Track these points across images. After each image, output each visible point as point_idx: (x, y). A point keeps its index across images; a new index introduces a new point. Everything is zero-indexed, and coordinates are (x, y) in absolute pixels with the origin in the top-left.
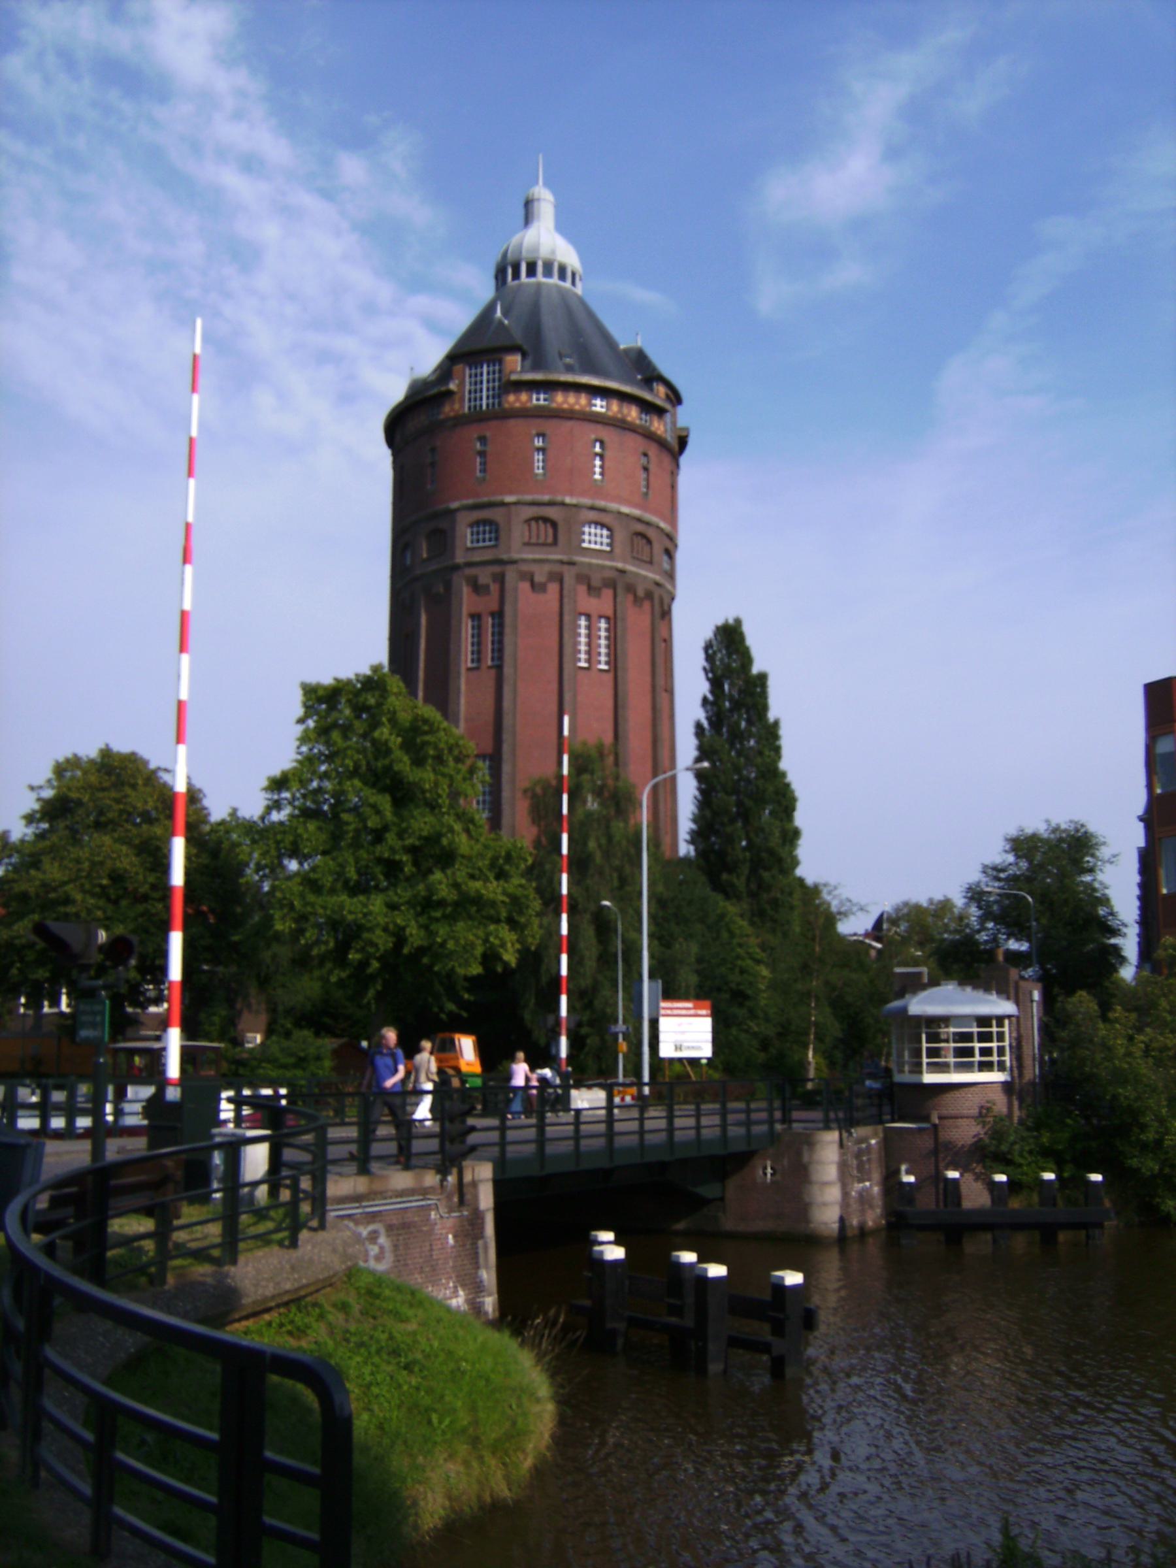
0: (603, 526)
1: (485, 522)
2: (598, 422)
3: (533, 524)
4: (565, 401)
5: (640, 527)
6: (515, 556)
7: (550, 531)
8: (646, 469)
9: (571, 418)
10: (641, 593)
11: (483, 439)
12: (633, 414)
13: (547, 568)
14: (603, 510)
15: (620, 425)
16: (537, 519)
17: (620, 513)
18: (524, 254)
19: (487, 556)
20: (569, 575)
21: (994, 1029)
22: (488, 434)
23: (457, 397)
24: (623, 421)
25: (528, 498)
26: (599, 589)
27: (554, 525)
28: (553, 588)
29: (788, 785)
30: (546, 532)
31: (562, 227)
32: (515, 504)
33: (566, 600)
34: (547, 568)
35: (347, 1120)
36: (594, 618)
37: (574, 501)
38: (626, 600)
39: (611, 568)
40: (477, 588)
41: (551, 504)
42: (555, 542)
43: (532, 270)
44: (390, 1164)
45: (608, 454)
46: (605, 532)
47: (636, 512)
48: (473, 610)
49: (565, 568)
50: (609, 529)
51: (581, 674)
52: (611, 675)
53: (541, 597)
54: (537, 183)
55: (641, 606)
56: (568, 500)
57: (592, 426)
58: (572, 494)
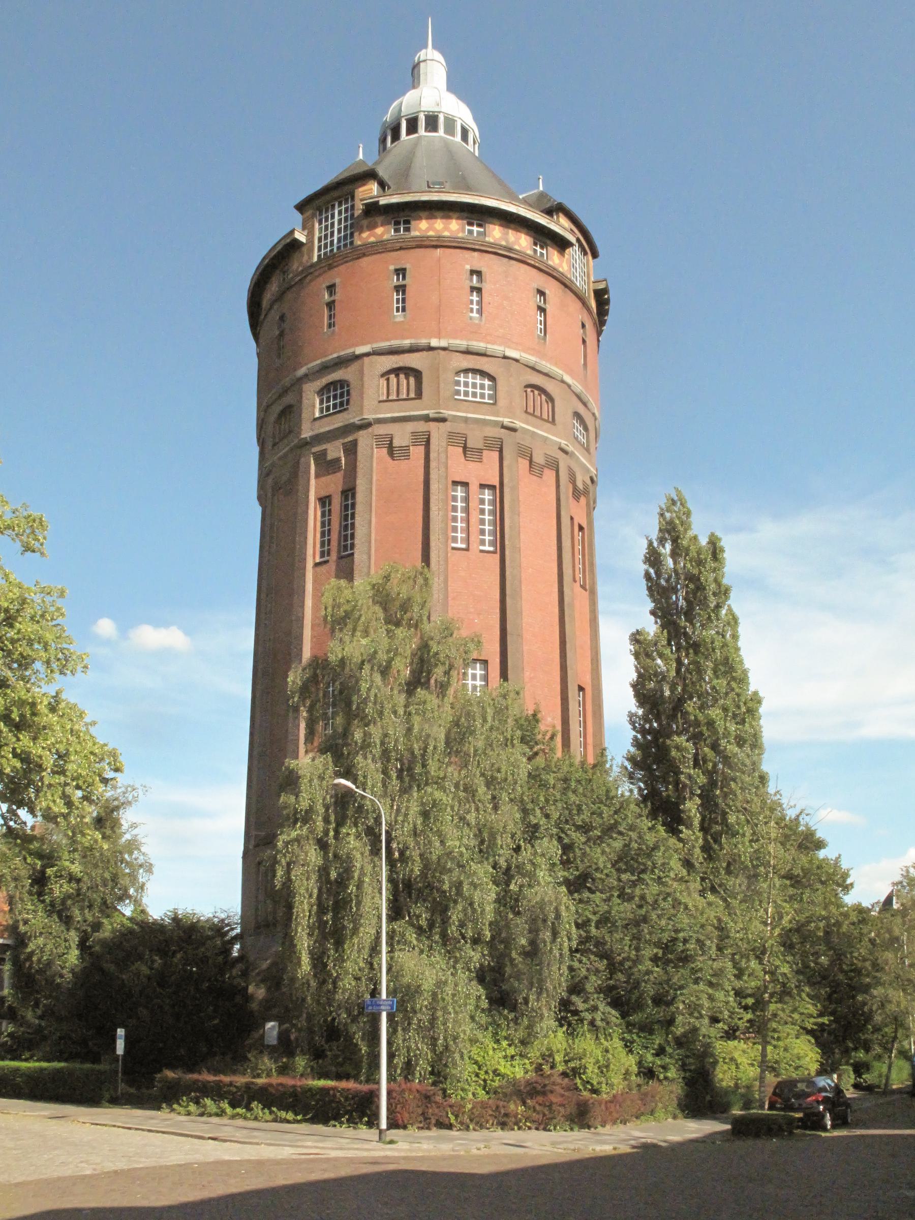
0: (483, 374)
1: (334, 384)
3: (392, 377)
6: (370, 416)
7: (412, 380)
8: (542, 310)
10: (539, 458)
11: (331, 288)
12: (523, 242)
13: (410, 427)
15: (508, 254)
16: (397, 371)
18: (404, 111)
19: (338, 422)
20: (438, 432)
21: (462, 389)
22: (337, 281)
23: (305, 249)
25: (384, 344)
26: (480, 451)
27: (417, 374)
28: (418, 452)
29: (159, 1108)
30: (406, 384)
31: (452, 87)
32: (367, 355)
33: (433, 464)
36: (474, 488)
37: (443, 343)
38: (517, 468)
39: (495, 423)
40: (327, 466)
41: (413, 350)
42: (419, 395)
43: (413, 126)
45: (486, 287)
46: (487, 382)
47: (531, 359)
48: (323, 494)
49: (433, 426)
50: (492, 378)
51: (454, 557)
52: (497, 556)
53: (404, 464)
54: (426, 47)
55: (540, 476)
56: (434, 343)
57: (467, 254)
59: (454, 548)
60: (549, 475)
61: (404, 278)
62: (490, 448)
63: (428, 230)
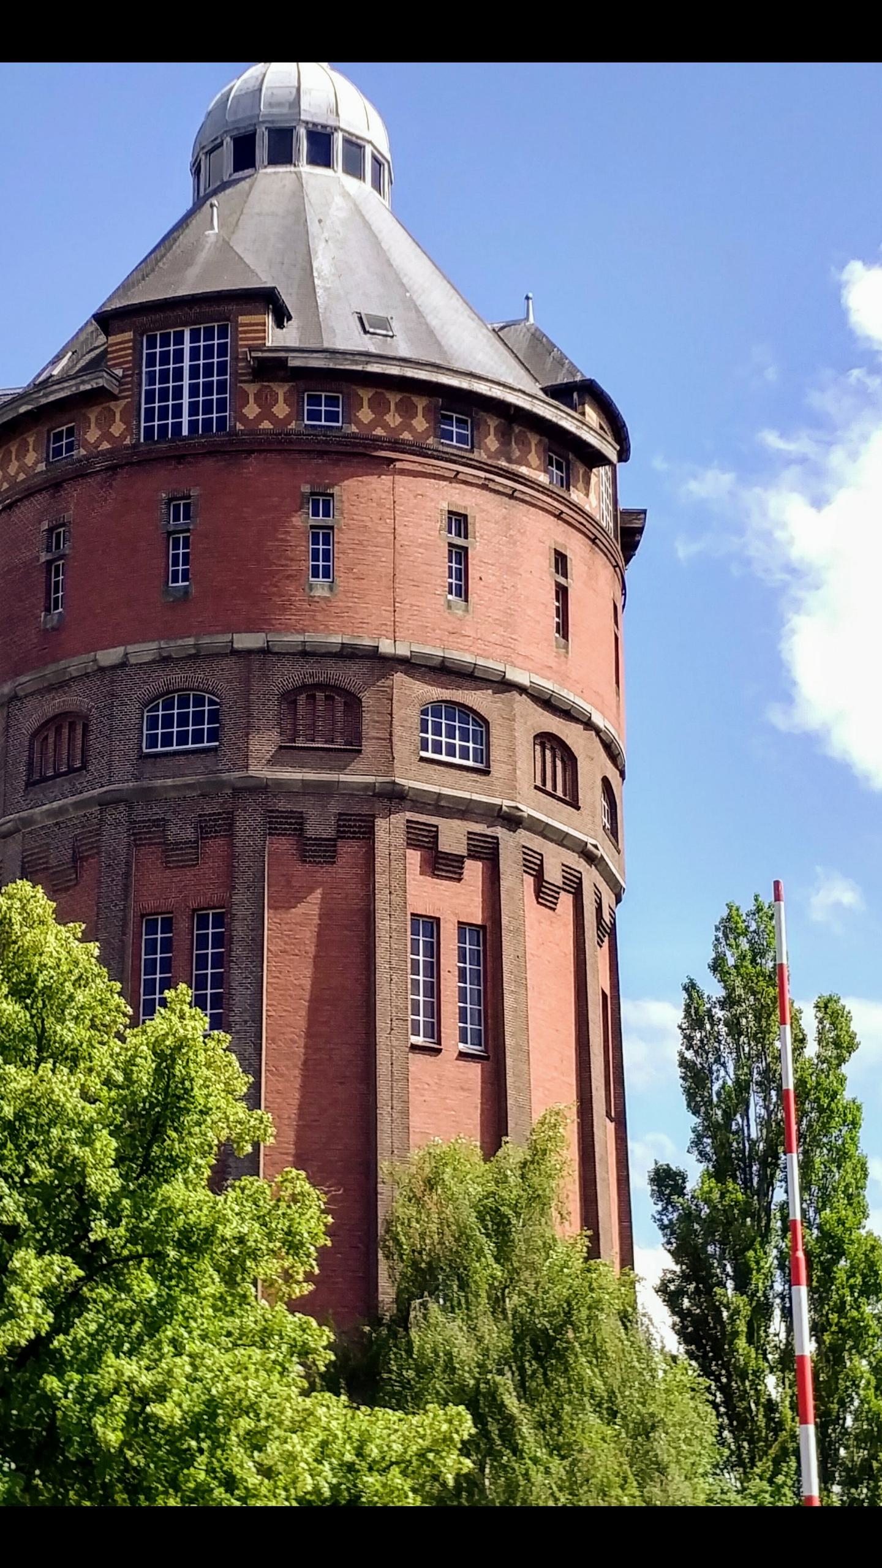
10: (553, 875)
16: (309, 689)
26: (460, 859)
32: (522, 689)
34: (334, 807)
51: (418, 1062)
59: (414, 1048)
60: (566, 901)
61: (327, 514)
62: (473, 855)
63: (374, 424)
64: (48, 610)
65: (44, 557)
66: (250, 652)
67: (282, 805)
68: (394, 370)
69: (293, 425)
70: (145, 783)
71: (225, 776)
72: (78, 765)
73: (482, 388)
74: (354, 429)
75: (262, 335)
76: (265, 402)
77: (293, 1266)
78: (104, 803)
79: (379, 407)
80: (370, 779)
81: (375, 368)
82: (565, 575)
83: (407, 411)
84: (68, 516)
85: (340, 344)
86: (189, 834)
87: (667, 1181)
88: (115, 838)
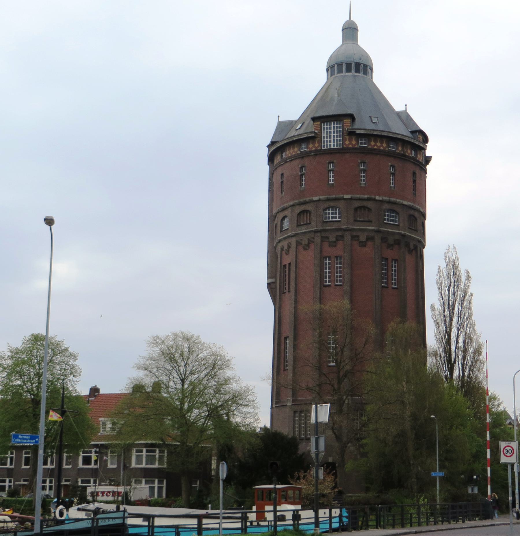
2: (390, 156)
4: (375, 145)
5: (357, 204)
9: (377, 154)
13: (366, 234)
14: (395, 203)
16: (360, 208)
17: (404, 205)
24: (379, 150)
34: (366, 234)
35: (174, 530)
41: (369, 199)
44: (374, 528)
56: (377, 198)
58: (379, 195)
63: (374, 146)
64: (301, 186)
65: (300, 174)
66: (347, 199)
67: (355, 234)
68: (379, 133)
69: (356, 146)
70: (325, 228)
71: (342, 227)
72: (308, 222)
73: (398, 136)
74: (370, 147)
75: (362, 66)
76: (350, 140)
77: (308, 389)
78: (315, 232)
79: (376, 141)
80: (373, 228)
81: (375, 133)
82: (415, 177)
83: (382, 143)
84: (306, 164)
85: (368, 127)
86: (334, 240)
87: (433, 308)
88: (318, 239)
